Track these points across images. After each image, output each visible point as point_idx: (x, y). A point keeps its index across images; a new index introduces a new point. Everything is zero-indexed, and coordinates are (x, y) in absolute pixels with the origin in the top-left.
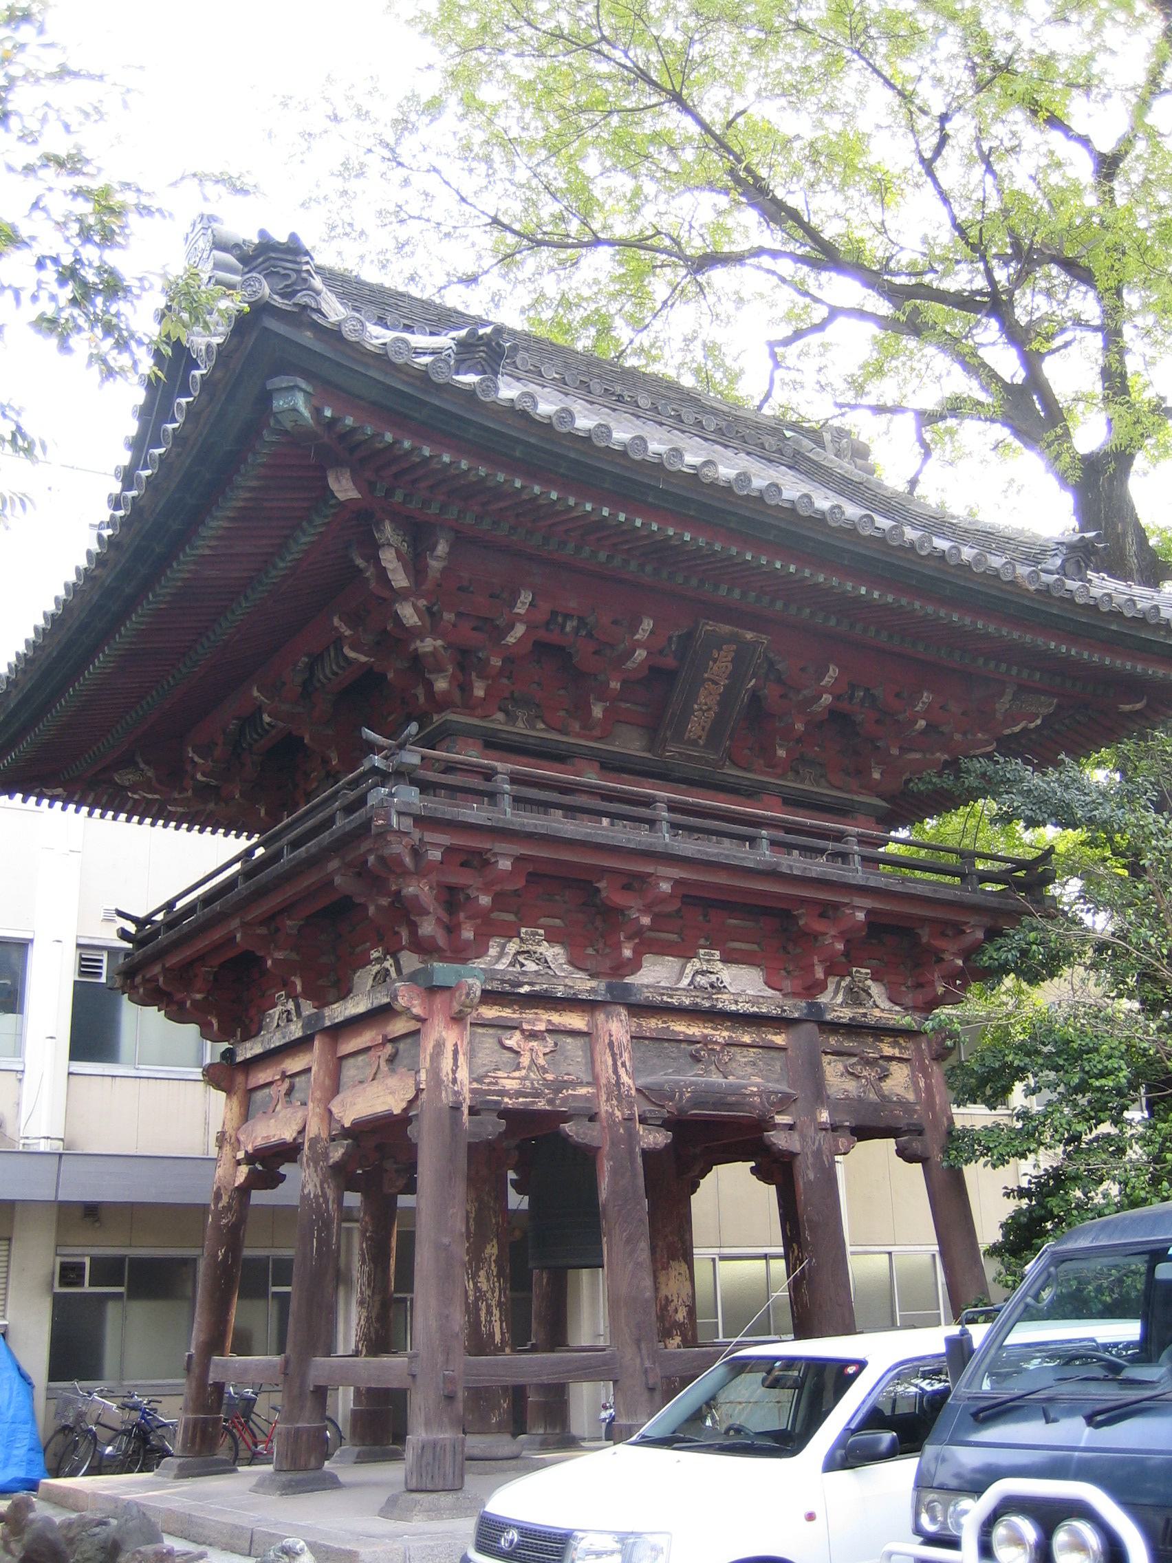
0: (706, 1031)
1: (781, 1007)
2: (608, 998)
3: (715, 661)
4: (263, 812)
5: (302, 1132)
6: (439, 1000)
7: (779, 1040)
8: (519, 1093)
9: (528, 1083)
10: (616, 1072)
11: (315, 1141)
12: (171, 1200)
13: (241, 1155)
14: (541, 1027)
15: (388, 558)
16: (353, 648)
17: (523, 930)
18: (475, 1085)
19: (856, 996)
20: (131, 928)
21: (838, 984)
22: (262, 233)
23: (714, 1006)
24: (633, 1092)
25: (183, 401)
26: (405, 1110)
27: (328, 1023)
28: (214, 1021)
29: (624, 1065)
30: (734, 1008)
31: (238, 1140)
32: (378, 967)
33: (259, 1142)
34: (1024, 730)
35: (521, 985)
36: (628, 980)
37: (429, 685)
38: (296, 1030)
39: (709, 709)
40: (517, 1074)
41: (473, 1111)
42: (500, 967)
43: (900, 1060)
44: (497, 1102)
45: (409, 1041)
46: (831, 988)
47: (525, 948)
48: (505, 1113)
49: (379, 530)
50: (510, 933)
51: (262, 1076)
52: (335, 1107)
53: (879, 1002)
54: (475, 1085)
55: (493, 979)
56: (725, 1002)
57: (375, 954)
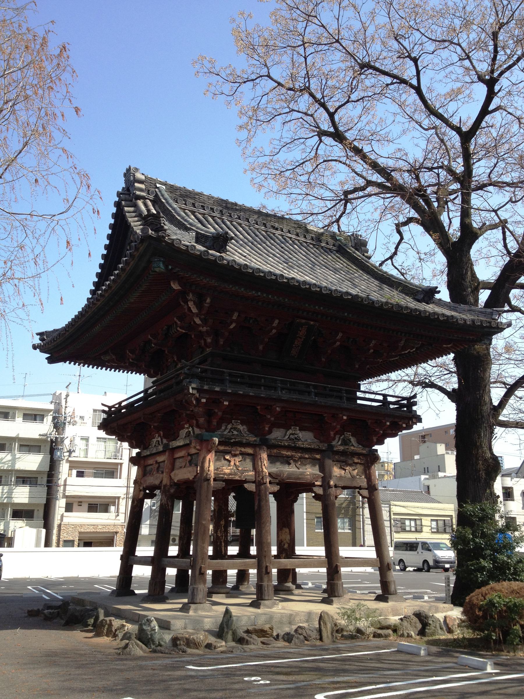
0: (293, 454)
1: (318, 446)
2: (260, 443)
3: (300, 331)
4: (152, 372)
5: (161, 482)
6: (204, 445)
7: (318, 456)
8: (230, 474)
9: (233, 471)
10: (262, 467)
11: (165, 486)
13: (141, 488)
14: (238, 452)
15: (191, 304)
16: (180, 328)
17: (233, 421)
18: (216, 472)
19: (346, 442)
20: (107, 409)
21: (340, 438)
23: (295, 446)
24: (267, 474)
25: (124, 259)
26: (193, 479)
27: (171, 447)
28: (134, 442)
29: (264, 465)
30: (302, 446)
31: (141, 483)
32: (187, 430)
33: (148, 484)
34: (409, 352)
35: (232, 439)
36: (267, 437)
37: (205, 340)
38: (161, 448)
39: (299, 346)
40: (229, 468)
41: (215, 480)
42: (225, 433)
43: (360, 464)
44: (223, 477)
45: (196, 455)
46: (337, 439)
47: (234, 427)
49: (188, 296)
51: (150, 461)
52: (172, 475)
53: (354, 444)
54: (216, 472)
55: (222, 438)
56: (300, 444)
57: (186, 426)
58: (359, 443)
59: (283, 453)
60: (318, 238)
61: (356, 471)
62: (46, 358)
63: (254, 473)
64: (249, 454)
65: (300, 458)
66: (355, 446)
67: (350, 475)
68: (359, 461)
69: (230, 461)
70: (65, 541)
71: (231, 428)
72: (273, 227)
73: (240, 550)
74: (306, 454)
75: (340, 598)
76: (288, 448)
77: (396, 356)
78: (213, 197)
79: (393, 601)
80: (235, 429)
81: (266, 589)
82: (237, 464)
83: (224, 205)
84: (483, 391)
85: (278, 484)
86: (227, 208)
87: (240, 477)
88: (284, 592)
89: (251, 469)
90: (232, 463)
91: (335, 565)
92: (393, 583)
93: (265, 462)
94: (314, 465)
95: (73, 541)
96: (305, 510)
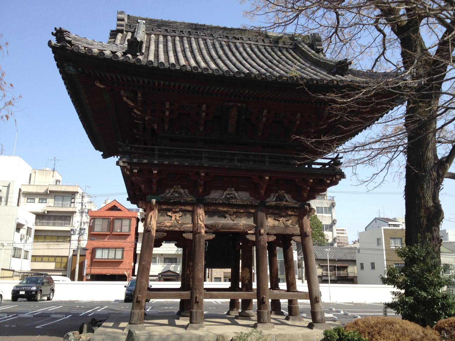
7: (252, 211)
8: (170, 227)
9: (173, 224)
12: (281, 233)
14: (178, 210)
18: (158, 225)
22: (60, 28)
29: (200, 219)
30: (236, 203)
35: (171, 200)
39: (233, 125)
41: (157, 231)
43: (294, 215)
47: (176, 190)
48: (166, 231)
50: (172, 187)
53: (288, 199)
54: (158, 225)
56: (233, 201)
58: (293, 198)
59: (220, 209)
60: (277, 40)
61: (290, 221)
62: (102, 155)
63: (192, 225)
64: (189, 211)
65: (235, 213)
66: (289, 200)
67: (283, 225)
68: (293, 213)
69: (171, 217)
70: (215, 278)
71: (174, 192)
72: (235, 38)
73: (182, 284)
74: (242, 209)
75: (264, 324)
76: (223, 205)
77: (324, 125)
78: (184, 23)
79: (318, 328)
80: (177, 192)
81: (195, 315)
82: (178, 218)
83: (194, 27)
84: (426, 148)
85: (213, 233)
86: (196, 29)
87: (179, 228)
88: (243, 318)
89: (191, 222)
90: (173, 218)
91: (261, 298)
92: (320, 313)
93: (201, 217)
94: (249, 217)
95: (220, 278)
96: (385, 259)
